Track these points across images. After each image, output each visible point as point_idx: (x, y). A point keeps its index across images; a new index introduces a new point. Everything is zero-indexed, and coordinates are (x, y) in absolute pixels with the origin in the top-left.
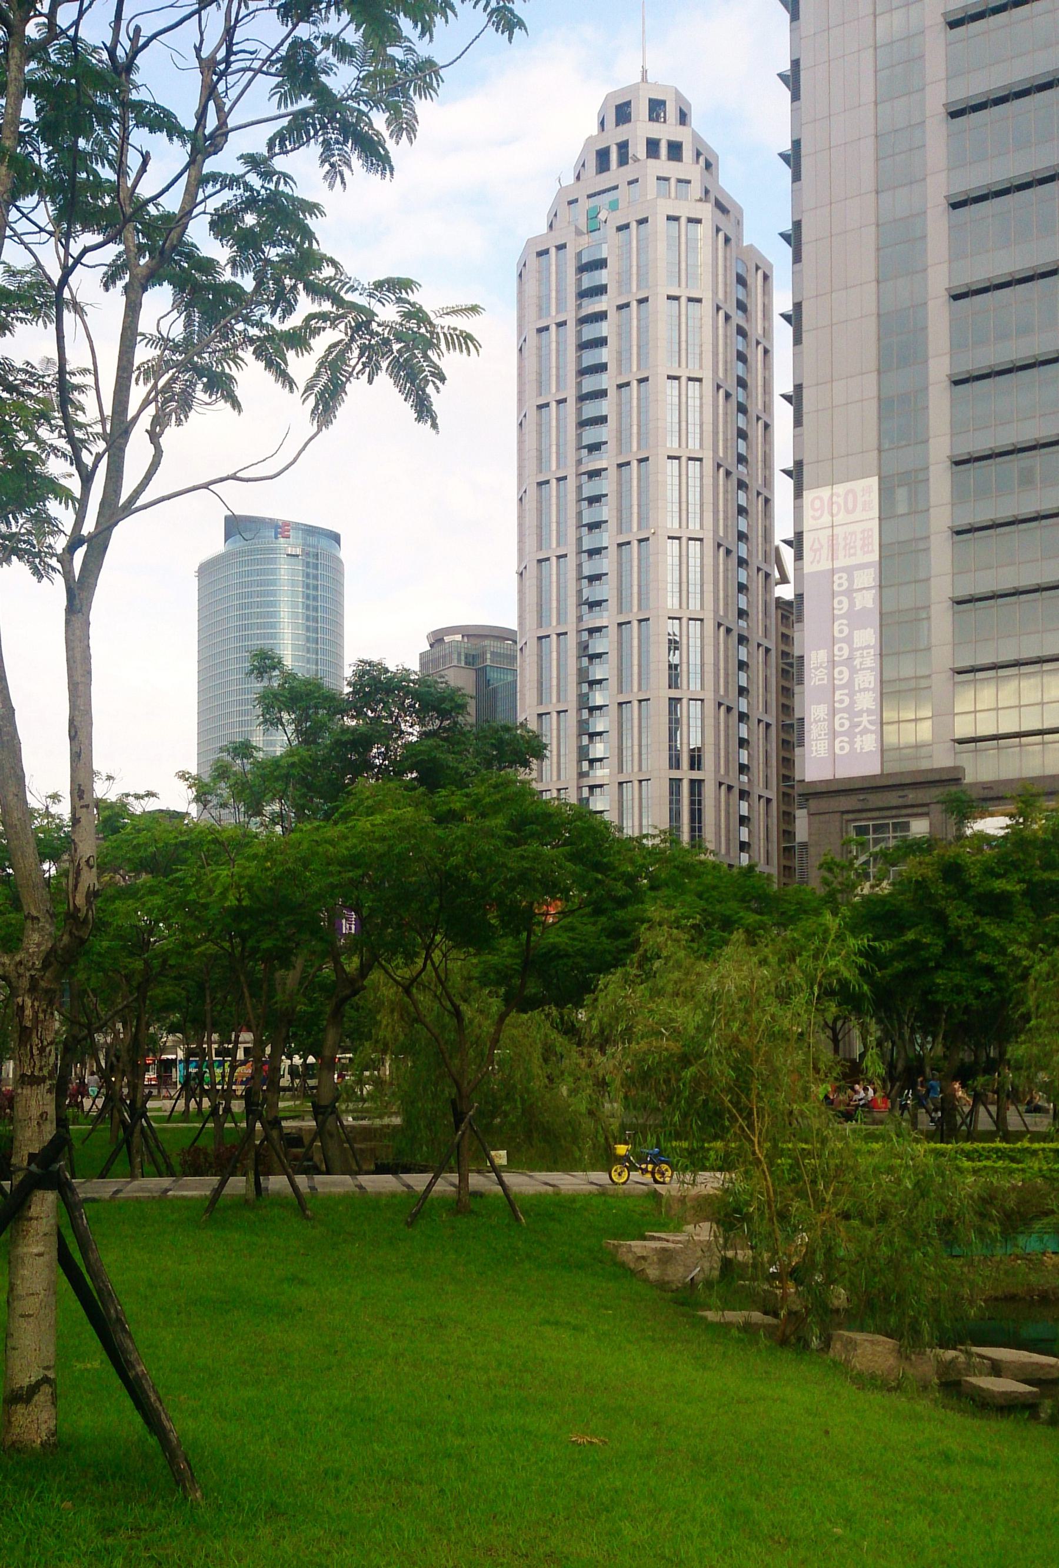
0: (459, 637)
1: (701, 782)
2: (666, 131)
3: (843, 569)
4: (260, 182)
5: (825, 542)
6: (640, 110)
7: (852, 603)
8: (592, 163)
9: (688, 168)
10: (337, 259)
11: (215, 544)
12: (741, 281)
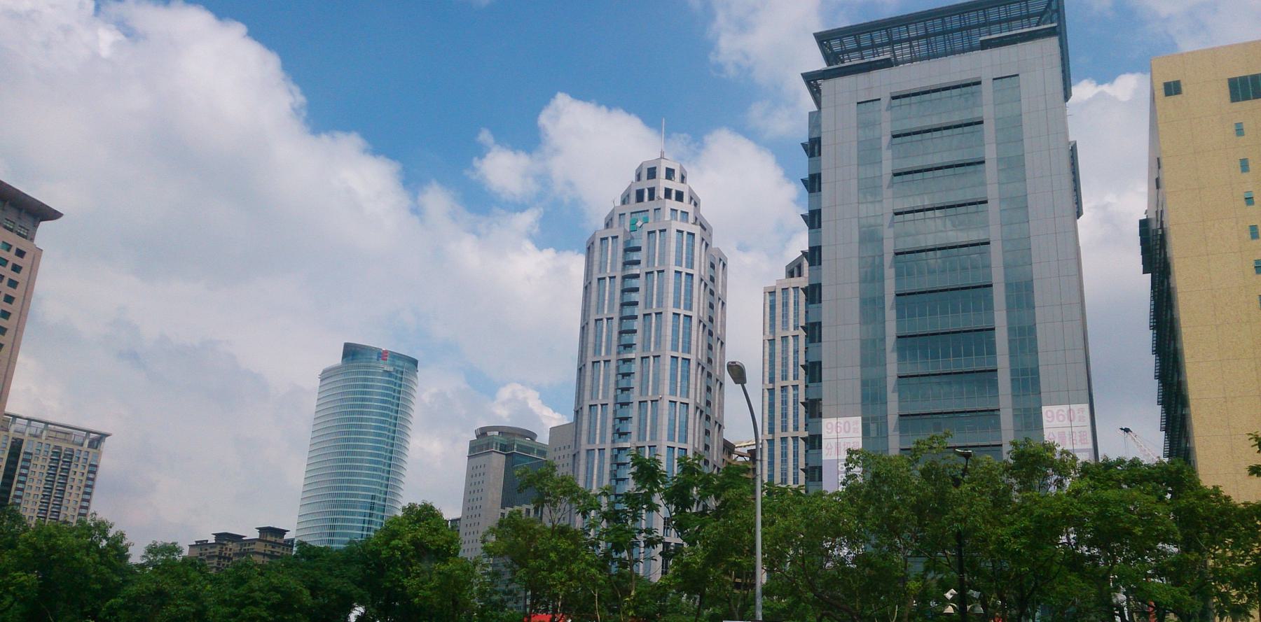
0: (496, 433)
1: (8, 250)
2: (675, 185)
5: (834, 445)
6: (662, 173)
8: (633, 197)
9: (685, 206)
11: (336, 359)
12: (712, 266)
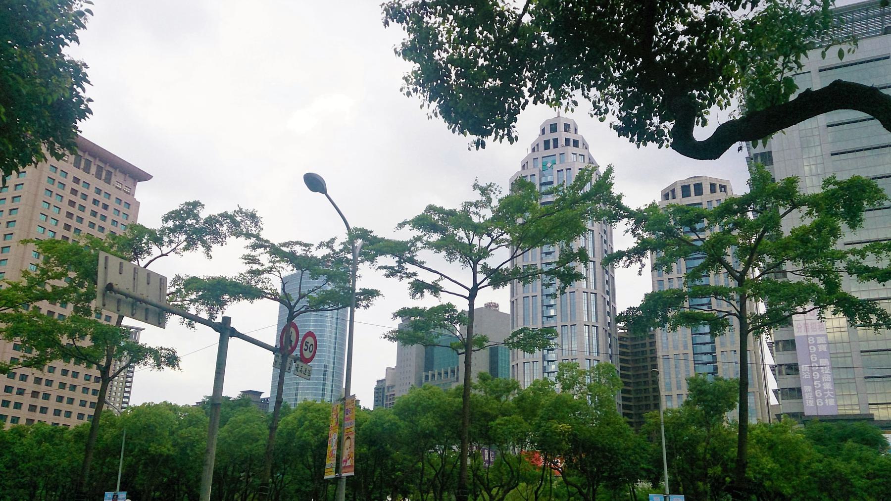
2: (571, 136)
3: (813, 336)
4: (420, 278)
6: (561, 128)
7: (817, 349)
10: (299, 240)
